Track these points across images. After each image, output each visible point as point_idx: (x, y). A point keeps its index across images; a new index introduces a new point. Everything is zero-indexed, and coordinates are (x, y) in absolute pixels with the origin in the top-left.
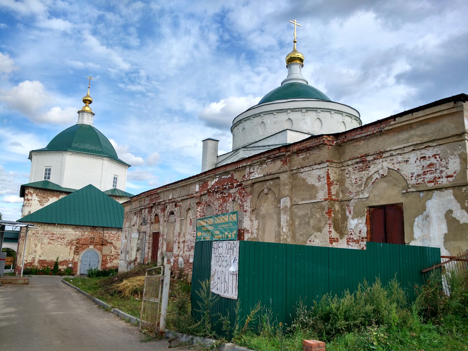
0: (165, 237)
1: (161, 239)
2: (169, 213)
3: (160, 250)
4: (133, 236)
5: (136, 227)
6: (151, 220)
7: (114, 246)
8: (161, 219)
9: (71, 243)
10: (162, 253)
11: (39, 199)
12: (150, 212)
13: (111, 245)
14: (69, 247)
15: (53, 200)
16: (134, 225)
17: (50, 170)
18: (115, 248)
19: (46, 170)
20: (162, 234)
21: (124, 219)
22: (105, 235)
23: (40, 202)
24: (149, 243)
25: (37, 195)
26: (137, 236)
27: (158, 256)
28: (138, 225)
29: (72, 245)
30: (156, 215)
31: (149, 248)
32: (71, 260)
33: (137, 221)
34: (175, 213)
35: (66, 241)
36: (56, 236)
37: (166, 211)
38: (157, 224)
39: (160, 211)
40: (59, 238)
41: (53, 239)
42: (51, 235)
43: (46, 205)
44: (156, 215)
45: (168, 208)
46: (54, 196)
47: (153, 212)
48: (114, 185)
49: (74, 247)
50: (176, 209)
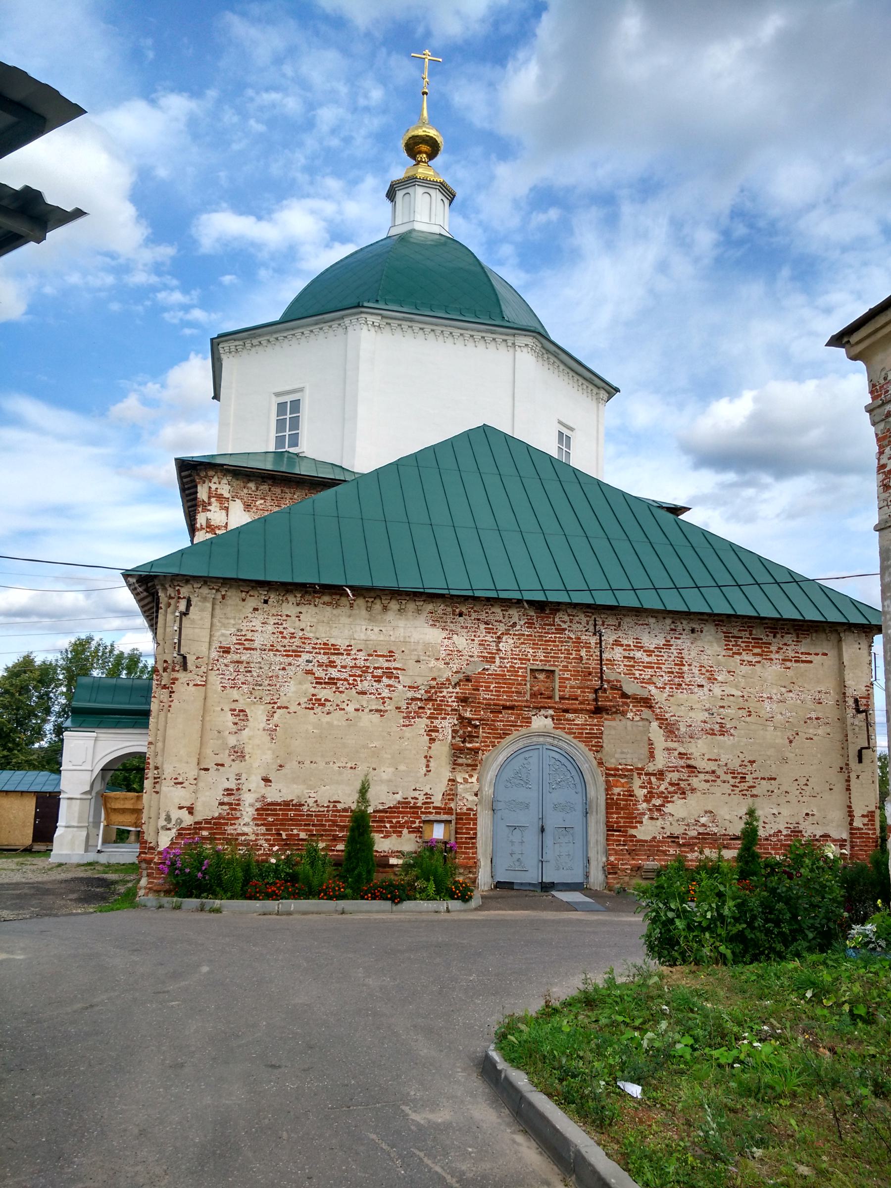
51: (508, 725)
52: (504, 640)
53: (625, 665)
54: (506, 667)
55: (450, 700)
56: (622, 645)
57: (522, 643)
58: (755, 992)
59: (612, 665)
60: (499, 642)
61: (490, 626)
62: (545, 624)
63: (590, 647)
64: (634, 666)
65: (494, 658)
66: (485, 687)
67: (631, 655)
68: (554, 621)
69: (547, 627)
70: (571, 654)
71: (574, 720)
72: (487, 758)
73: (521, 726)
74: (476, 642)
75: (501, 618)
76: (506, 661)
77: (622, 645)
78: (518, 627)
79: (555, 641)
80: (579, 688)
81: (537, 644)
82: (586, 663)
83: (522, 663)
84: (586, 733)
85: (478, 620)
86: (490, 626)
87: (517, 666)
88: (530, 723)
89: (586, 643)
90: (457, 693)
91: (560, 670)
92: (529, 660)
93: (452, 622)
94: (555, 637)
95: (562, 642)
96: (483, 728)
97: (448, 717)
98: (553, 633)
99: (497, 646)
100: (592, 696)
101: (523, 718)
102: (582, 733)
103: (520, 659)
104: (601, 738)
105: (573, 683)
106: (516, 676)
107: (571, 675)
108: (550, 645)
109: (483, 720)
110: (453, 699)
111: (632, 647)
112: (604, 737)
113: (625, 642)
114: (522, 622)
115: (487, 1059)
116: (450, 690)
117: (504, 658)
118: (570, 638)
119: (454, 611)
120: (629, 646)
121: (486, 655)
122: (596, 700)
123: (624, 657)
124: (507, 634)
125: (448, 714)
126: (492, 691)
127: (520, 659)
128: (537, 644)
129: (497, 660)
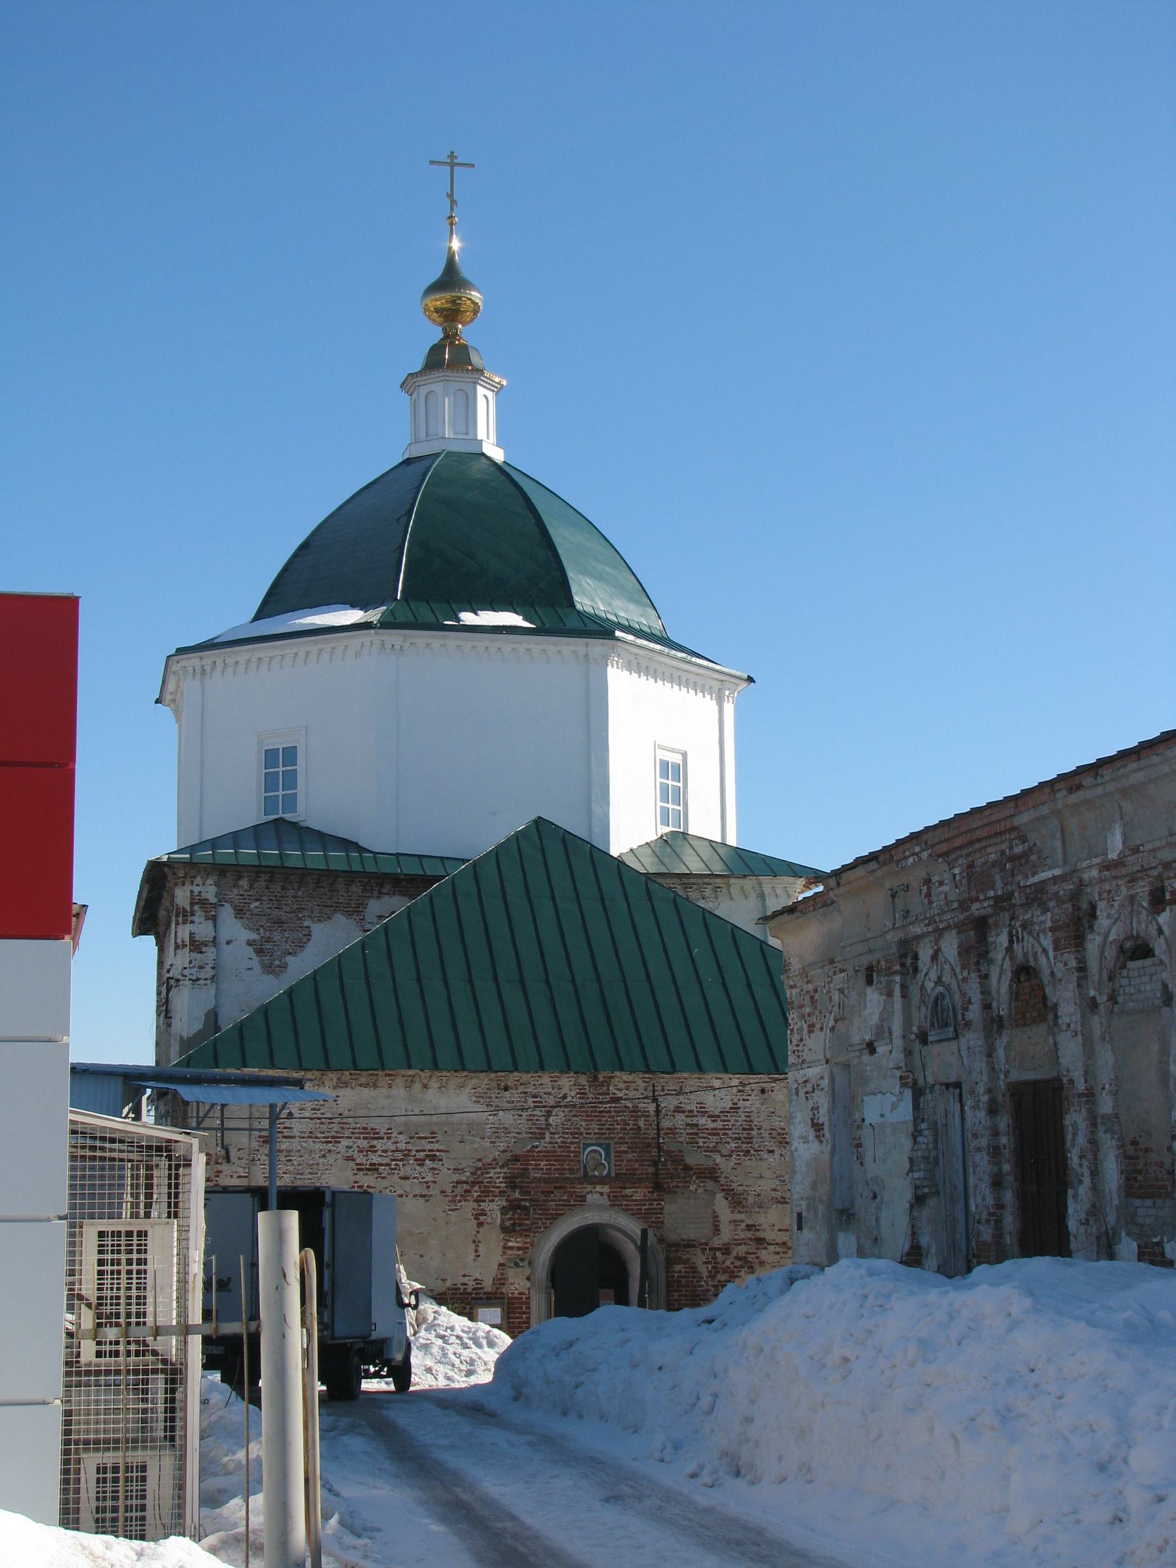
0: (1106, 1106)
1: (1075, 1119)
2: (1111, 953)
3: (1084, 1190)
4: (871, 1116)
5: (890, 1054)
6: (987, 1006)
7: (728, 1192)
8: (1066, 999)
9: (474, 1185)
10: (1095, 1211)
11: (253, 936)
12: (976, 951)
13: (710, 1184)
14: (468, 1207)
15: (330, 938)
16: (871, 1048)
17: (290, 754)
18: (736, 1201)
19: (271, 757)
20: (1081, 1086)
21: (792, 1016)
22: (666, 1124)
23: (260, 952)
24: (995, 1151)
25: (239, 912)
26: (905, 1112)
27: (1072, 1225)
28: (898, 1042)
29: (486, 1193)
30: (1024, 972)
31: (997, 1183)
32: (488, 1285)
33: (886, 1015)
34: (1159, 947)
35: (446, 1177)
36: (390, 1146)
37: (1093, 944)
38: (1041, 1029)
39: (1047, 941)
40: (407, 1154)
41: (374, 1168)
42: (363, 1144)
43: (302, 965)
44: (1024, 972)
45: (1103, 922)
46: (337, 908)
47: (999, 955)
48: (665, 813)
49: (494, 1208)
50: (1164, 918)
56: (684, 1112)
64: (696, 1134)
77: (684, 1112)
78: (569, 1099)
80: (636, 1161)
98: (608, 1102)
99: (547, 1120)
100: (651, 1170)
105: (630, 1156)
112: (665, 1211)
114: (573, 1094)
116: (498, 1170)
120: (691, 1111)
122: (656, 1174)
123: (687, 1125)
129: (548, 1136)
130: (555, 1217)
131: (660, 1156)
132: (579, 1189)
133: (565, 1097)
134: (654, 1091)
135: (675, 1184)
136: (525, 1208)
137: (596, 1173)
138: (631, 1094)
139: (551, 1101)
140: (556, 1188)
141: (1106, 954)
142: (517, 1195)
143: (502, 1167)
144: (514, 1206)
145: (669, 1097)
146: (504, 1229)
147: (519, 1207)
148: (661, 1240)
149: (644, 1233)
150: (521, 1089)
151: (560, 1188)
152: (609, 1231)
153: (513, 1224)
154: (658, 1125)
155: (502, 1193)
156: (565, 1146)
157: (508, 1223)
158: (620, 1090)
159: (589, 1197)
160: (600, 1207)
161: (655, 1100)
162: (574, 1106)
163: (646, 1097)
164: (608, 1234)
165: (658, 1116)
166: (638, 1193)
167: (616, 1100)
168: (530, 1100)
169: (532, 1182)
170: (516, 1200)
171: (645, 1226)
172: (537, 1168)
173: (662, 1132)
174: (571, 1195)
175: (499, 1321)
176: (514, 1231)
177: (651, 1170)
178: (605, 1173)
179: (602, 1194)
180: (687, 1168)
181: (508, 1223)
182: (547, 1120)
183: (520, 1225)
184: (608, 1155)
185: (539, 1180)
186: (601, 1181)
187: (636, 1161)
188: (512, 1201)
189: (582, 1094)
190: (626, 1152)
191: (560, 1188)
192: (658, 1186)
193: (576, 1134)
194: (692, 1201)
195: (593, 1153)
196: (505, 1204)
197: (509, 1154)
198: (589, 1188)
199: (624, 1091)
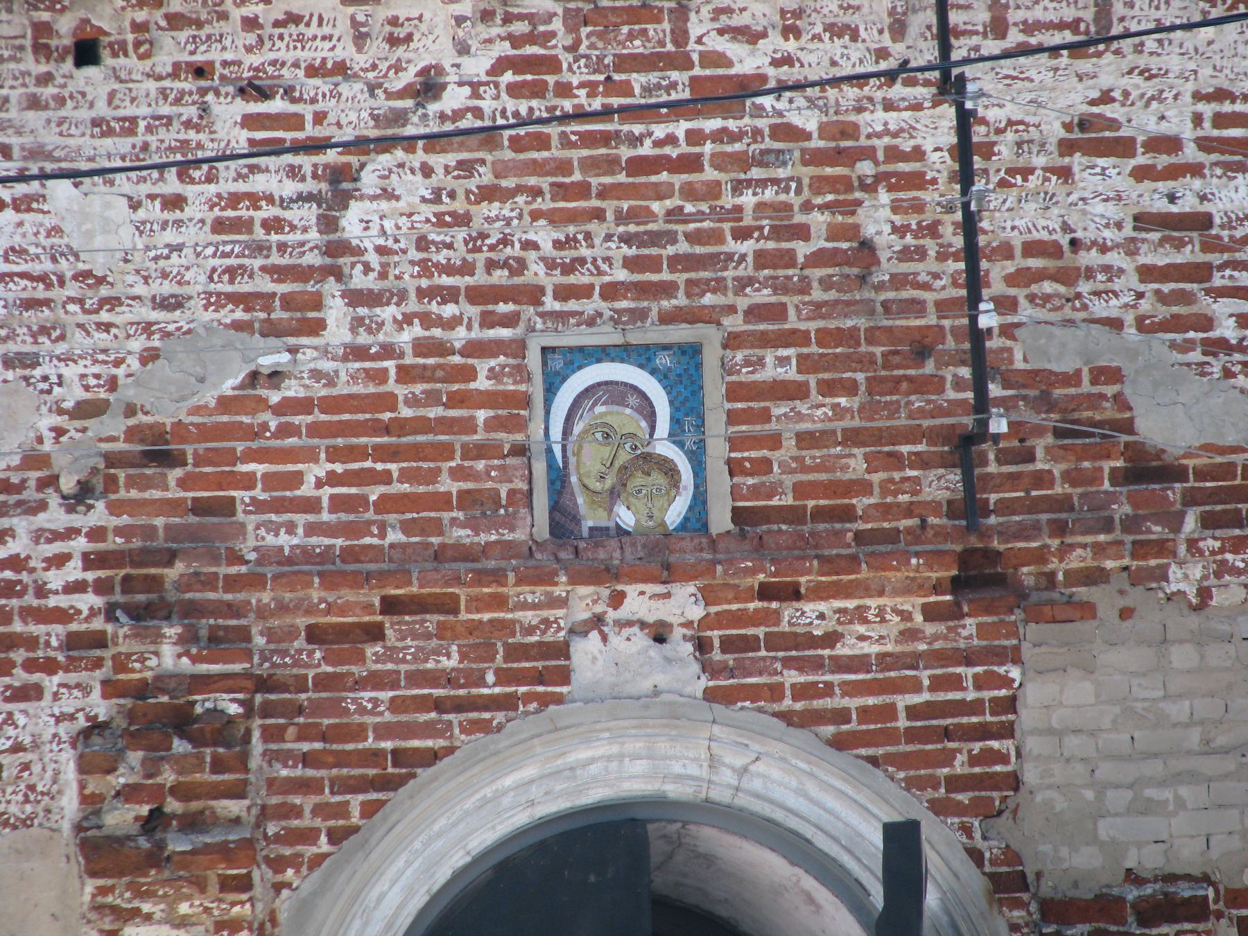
22: (1013, 218)
51: (423, 704)
52: (369, 181)
53: (1147, 273)
54: (388, 351)
55: (55, 579)
56: (1123, 148)
57: (488, 194)
58: (48, 342)
59: (1067, 276)
60: (342, 200)
61: (277, 105)
62: (624, 63)
63: (918, 181)
64: (1200, 273)
65: (317, 302)
66: (270, 481)
67: (1188, 204)
68: (680, 36)
69: (638, 80)
70: (802, 232)
71: (831, 639)
72: (304, 910)
73: (506, 704)
74: (193, 210)
75: (345, 51)
76: (388, 313)
77: (1123, 148)
78: (454, 98)
79: (691, 163)
80: (853, 438)
81: (582, 190)
82: (899, 281)
83: (489, 321)
84: (912, 712)
85: (200, 71)
86: (277, 105)
87: (460, 336)
88: (564, 676)
89: (894, 154)
90: (96, 534)
91: (732, 341)
92: (534, 295)
93: (34, 103)
94: (695, 137)
95: (743, 162)
96: (270, 734)
97: (51, 683)
98: (677, 109)
99: (328, 224)
100: (940, 485)
101: (515, 652)
102: (889, 712)
103: (476, 295)
104: (1007, 731)
105: (817, 412)
106: (457, 400)
107: (805, 364)
108: (660, 193)
109: (264, 684)
110: (74, 571)
111: (1191, 153)
112: (1027, 717)
113: (1143, 123)
114: (477, 66)
115: (238, 616)
116: (55, 516)
117: (373, 299)
118: (786, 132)
119: (42, 29)
120: (1171, 144)
121: (265, 285)
122: (968, 508)
123: (1143, 221)
124: (385, 144)
125: (50, 667)
126: (311, 505)
127: (476, 295)
128: (582, 190)
129: (336, 313)
130: (394, 772)
131: (982, 404)
132: (527, 609)
133: (428, 86)
134: (945, 35)
135: (1078, 560)
136: (222, 732)
137: (626, 517)
138: (817, 57)
139: (351, 113)
140: (391, 606)
141: (534, 788)
142: (168, 656)
143: (81, 497)
144: (157, 717)
145: (1038, 67)
146: (99, 852)
147: (181, 721)
148: (1008, 882)
149: (902, 843)
150: (172, 49)
151: (419, 605)
152: (710, 837)
153: (154, 822)
154: (970, 226)
155: (84, 645)
156: (436, 366)
157: (122, 818)
158: (751, 36)
159: (586, 651)
160: (652, 708)
161: (950, 86)
162: (488, 136)
163: (901, 72)
164: (709, 860)
165: (965, 177)
166: (877, 621)
167: (736, 93)
168: (229, 112)
169: (255, 581)
170: (161, 682)
171: (913, 807)
172: (284, 500)
173: (996, 272)
174: (480, 643)
175: (650, 827)
176: (156, 858)
177: (940, 485)
178: (675, 513)
179: (660, 634)
180: (1147, 469)
181: (122, 818)
182: (328, 224)
183: (192, 823)
184: (688, 410)
185: (292, 567)
186: (659, 559)
187: (853, 438)
188: (141, 690)
189: (529, 68)
190: (794, 392)
191: (419, 605)
192: (978, 578)
193: (504, 297)
194: (1182, 656)
195: (603, 418)
196: (102, 708)
197: (114, 425)
198: (585, 600)
199: (775, 43)
